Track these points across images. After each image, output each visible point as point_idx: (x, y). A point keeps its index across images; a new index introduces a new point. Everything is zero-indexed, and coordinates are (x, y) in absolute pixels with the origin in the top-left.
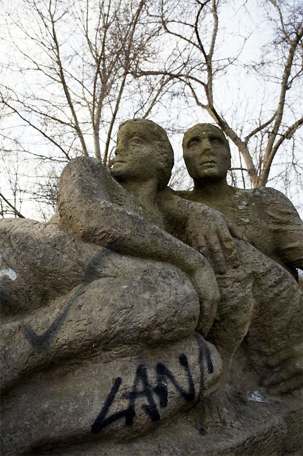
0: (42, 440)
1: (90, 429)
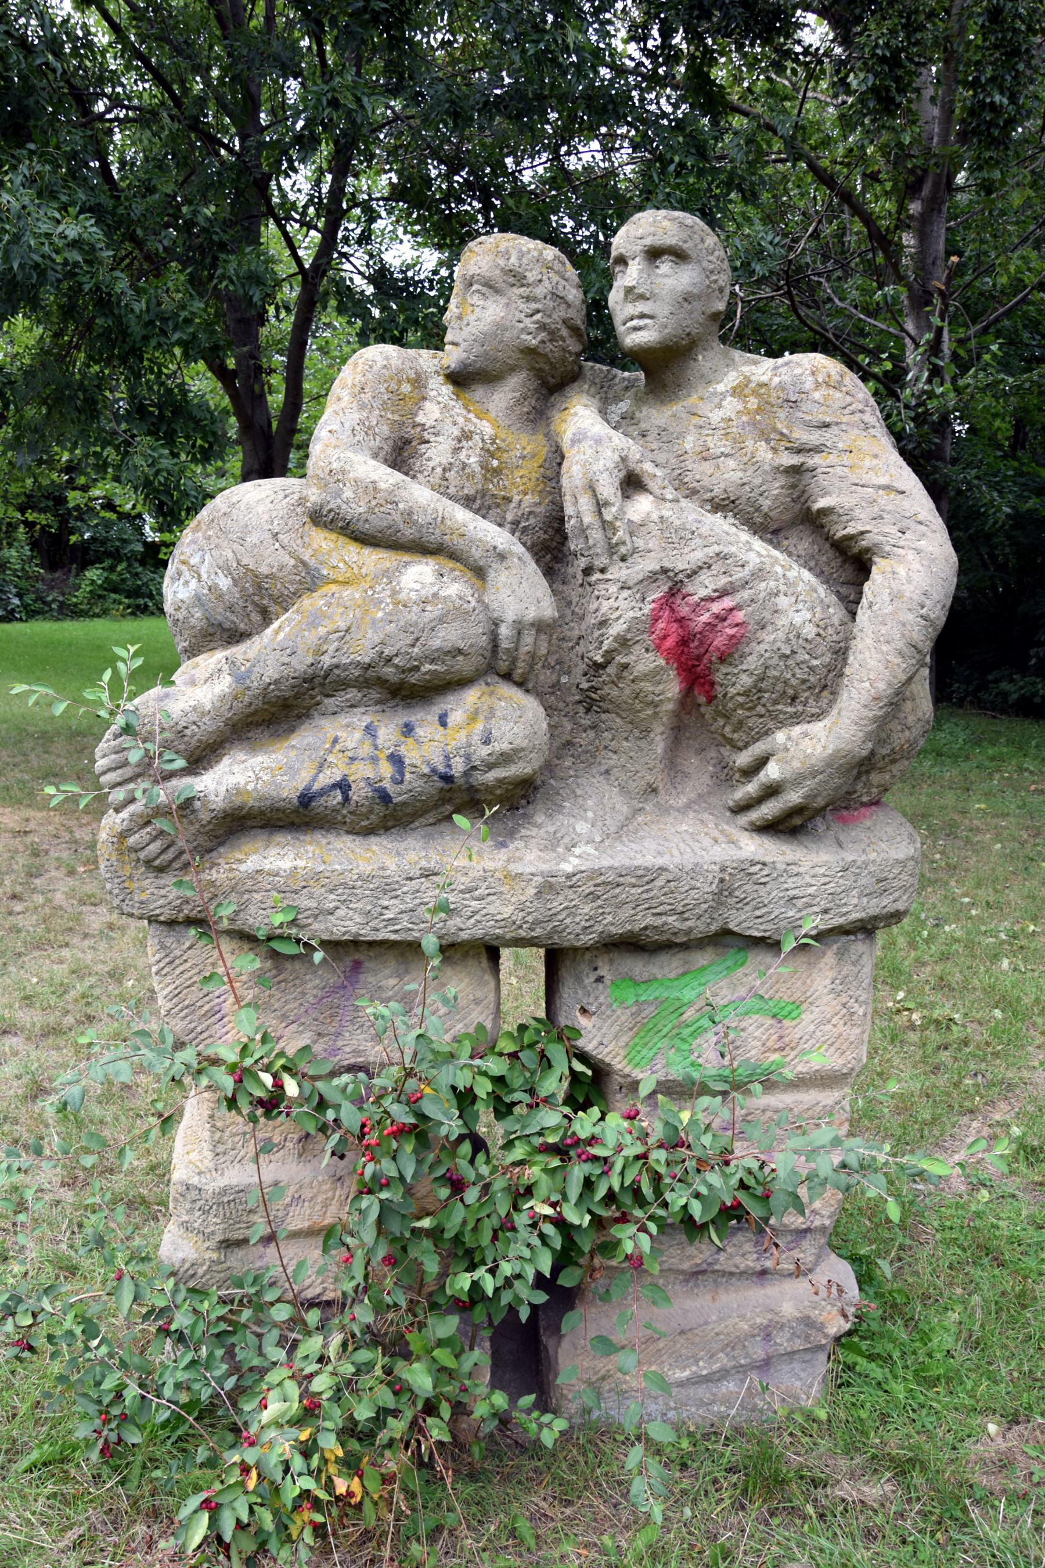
0: (241, 808)
1: (295, 801)
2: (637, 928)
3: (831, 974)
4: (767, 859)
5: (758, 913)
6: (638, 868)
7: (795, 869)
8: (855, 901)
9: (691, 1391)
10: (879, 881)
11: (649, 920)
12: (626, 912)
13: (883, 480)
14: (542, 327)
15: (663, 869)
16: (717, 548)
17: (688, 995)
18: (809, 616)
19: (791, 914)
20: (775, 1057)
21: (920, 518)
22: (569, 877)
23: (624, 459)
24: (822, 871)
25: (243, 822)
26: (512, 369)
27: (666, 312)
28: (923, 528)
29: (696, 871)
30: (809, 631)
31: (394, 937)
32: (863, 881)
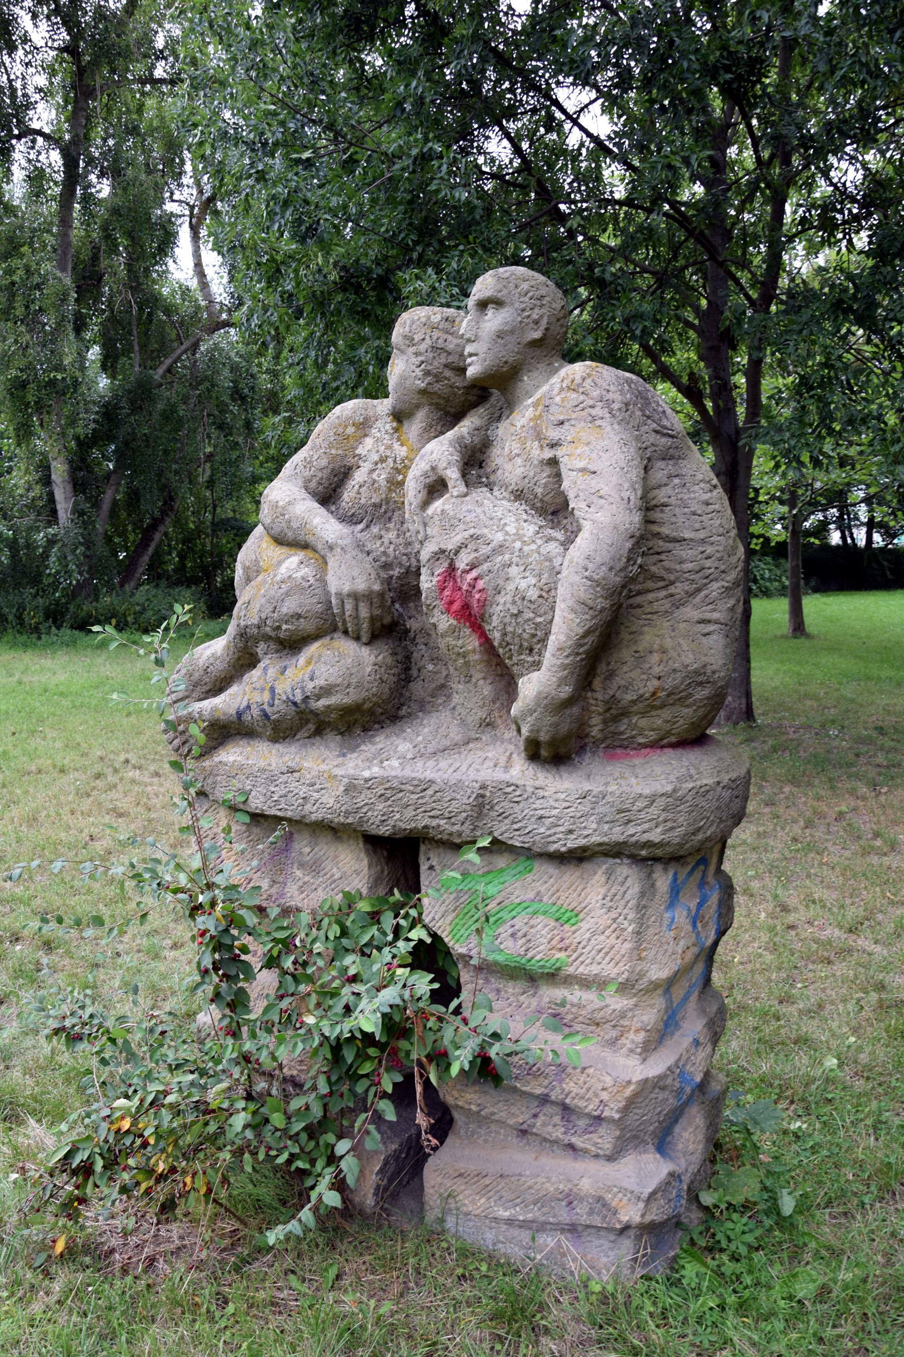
2: (420, 826)
3: (603, 891)
4: (519, 783)
5: (516, 826)
6: (413, 779)
7: (541, 793)
8: (594, 826)
9: (515, 1232)
10: (620, 811)
11: (427, 821)
12: (409, 813)
13: (581, 465)
14: (427, 373)
15: (432, 782)
16: (472, 531)
17: (491, 890)
18: (533, 581)
19: (542, 830)
20: (562, 955)
21: (602, 493)
22: (367, 780)
23: (433, 469)
24: (563, 796)
25: (223, 732)
26: (418, 407)
27: (485, 349)
28: (602, 501)
29: (458, 785)
30: (533, 594)
31: (279, 814)
32: (600, 809)
